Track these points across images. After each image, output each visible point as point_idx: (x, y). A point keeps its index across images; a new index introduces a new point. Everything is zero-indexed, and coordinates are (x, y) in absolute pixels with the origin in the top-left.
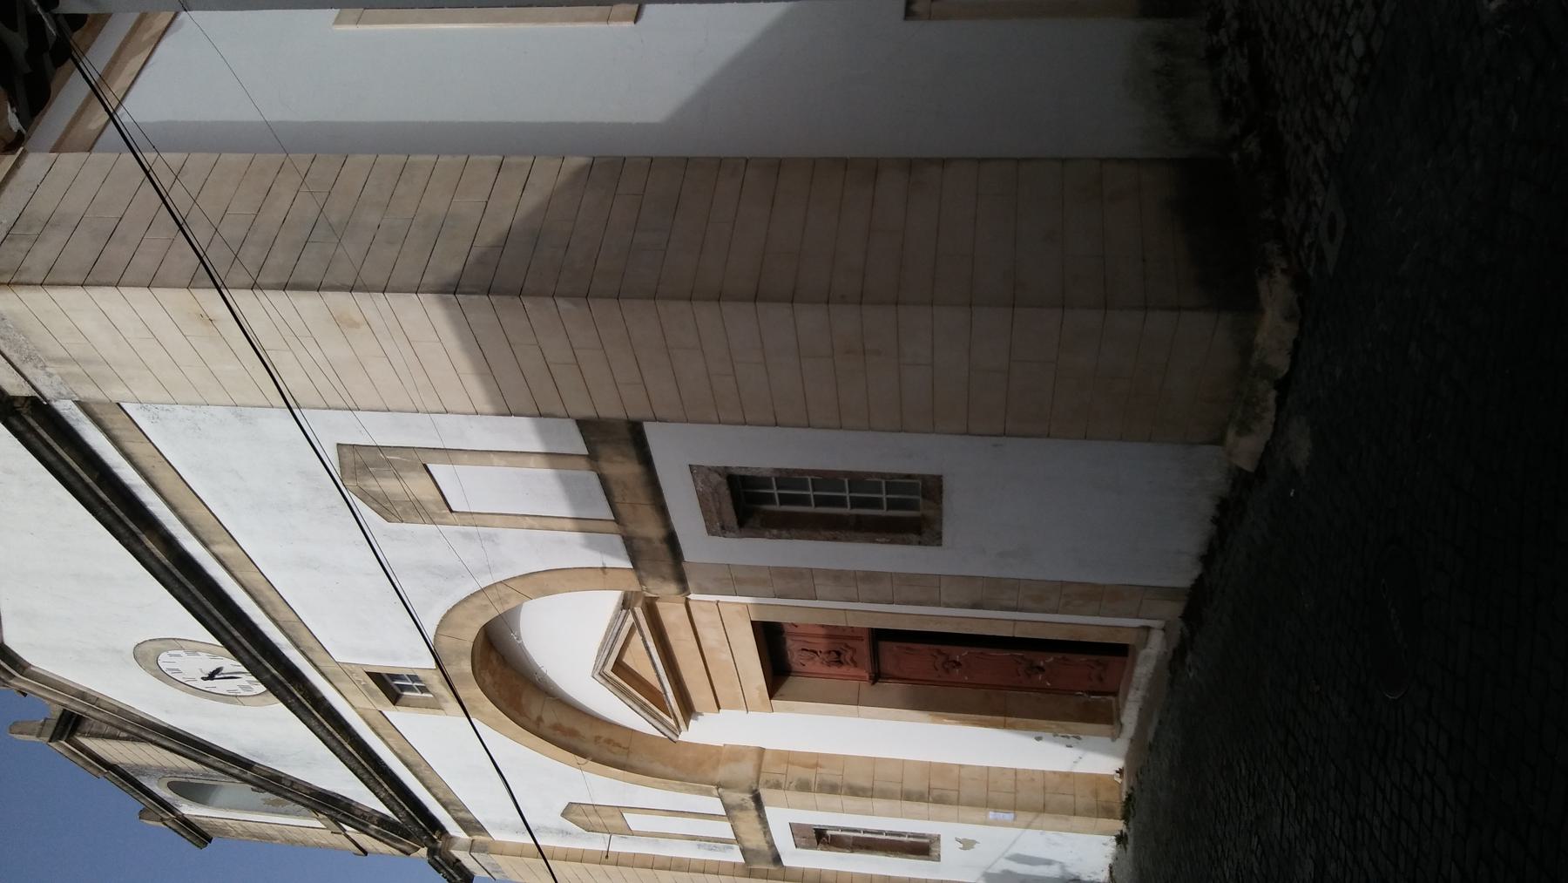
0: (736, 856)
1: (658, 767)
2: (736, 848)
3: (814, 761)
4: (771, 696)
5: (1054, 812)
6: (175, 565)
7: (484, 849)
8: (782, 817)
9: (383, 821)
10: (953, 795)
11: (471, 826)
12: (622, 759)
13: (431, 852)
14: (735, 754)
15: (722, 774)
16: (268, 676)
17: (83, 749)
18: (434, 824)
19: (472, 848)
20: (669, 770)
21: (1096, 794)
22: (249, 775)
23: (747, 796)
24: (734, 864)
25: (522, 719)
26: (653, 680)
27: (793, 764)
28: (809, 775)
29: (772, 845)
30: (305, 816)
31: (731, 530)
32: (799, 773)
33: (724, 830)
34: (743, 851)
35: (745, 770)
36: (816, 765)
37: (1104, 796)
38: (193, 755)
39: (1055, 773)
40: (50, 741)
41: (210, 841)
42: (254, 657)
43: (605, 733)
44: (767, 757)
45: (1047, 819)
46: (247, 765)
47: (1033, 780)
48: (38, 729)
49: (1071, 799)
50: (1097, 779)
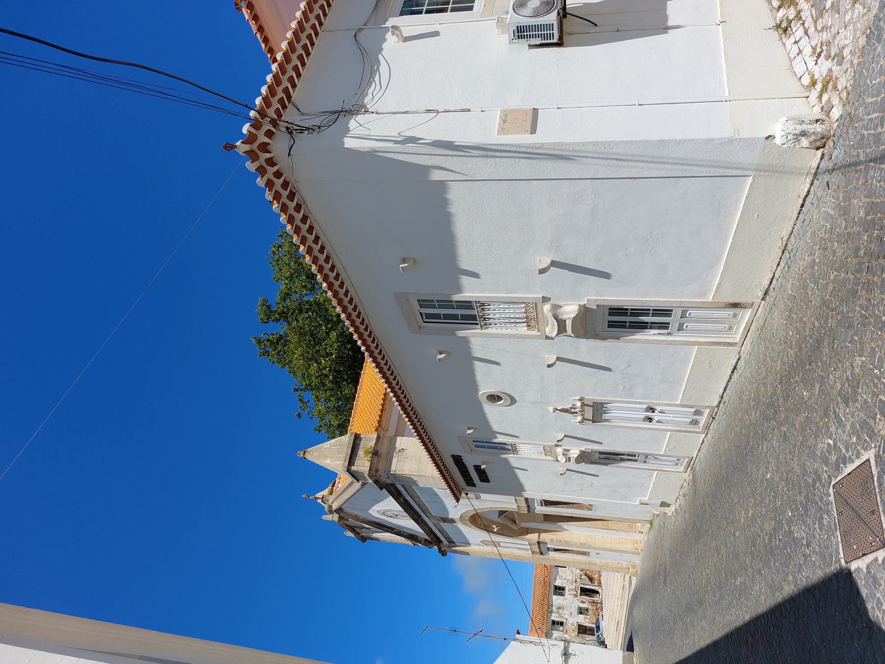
13: (440, 549)
18: (440, 541)
25: (477, 525)
33: (529, 547)
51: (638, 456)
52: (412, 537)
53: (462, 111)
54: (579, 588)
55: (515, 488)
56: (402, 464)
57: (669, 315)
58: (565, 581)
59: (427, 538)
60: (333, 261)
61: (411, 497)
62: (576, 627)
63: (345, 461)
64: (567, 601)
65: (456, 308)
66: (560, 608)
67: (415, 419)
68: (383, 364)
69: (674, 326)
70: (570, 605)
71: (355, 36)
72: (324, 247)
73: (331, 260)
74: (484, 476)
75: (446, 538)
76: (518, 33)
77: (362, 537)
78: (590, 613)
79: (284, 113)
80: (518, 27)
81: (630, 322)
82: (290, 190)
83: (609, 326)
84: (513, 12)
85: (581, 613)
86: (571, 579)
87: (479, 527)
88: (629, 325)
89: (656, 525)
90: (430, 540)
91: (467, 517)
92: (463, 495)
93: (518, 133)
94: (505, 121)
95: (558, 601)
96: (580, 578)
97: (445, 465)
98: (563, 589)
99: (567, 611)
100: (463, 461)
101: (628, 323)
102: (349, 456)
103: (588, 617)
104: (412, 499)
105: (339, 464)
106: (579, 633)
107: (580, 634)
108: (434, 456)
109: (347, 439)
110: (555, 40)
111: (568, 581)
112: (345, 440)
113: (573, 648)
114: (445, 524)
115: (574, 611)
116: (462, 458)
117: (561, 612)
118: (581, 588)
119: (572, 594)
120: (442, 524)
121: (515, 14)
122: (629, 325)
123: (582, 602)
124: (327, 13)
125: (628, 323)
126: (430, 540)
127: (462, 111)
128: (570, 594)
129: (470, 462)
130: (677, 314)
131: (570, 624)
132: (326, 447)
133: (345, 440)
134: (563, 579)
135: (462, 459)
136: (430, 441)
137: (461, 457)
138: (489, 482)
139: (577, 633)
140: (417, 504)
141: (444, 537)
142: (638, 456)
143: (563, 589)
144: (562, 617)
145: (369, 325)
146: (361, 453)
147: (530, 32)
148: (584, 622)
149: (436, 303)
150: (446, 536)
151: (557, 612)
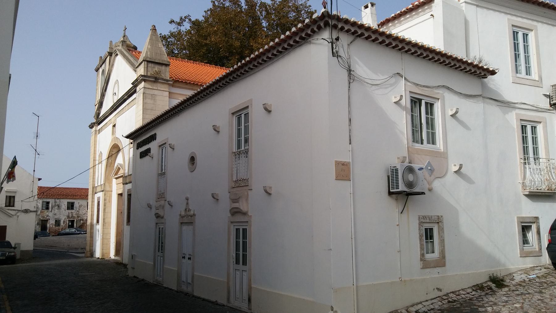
0: (96, 185)
1: (107, 172)
2: (97, 185)
3: (110, 201)
4: (118, 194)
5: (102, 246)
6: (124, 99)
7: (95, 133)
8: (100, 195)
9: (99, 114)
10: (105, 227)
11: (100, 131)
12: (108, 166)
13: (94, 123)
14: (111, 187)
15: (107, 184)
16: (114, 106)
17: (107, 56)
18: (99, 124)
19: (96, 131)
20: (107, 174)
21: (106, 253)
22: (104, 91)
23: (103, 189)
24: (95, 184)
25: (112, 149)
26: (119, 174)
27: (109, 197)
28: (107, 201)
29: (97, 193)
30: (100, 92)
31: (128, 193)
32: (108, 198)
33: (99, 184)
34: (96, 187)
35: (108, 188)
36: (109, 202)
37: (105, 255)
38: (105, 86)
39: (110, 246)
40: (108, 52)
41: (96, 72)
42: (116, 105)
43: (113, 162)
44: (111, 192)
45: (101, 245)
46: (106, 90)
47: (108, 242)
48: (111, 47)
49: (105, 249)
50: (109, 253)
51: (161, 252)
52: (101, 104)
53: (350, 140)
54: (74, 219)
55: (508, 19)
56: (150, 98)
57: (243, 264)
58: (78, 210)
59: (101, 115)
60: (290, 49)
61: (128, 104)
62: (46, 218)
63: (150, 58)
64: (64, 212)
65: (245, 136)
66: (59, 206)
67: (177, 109)
68: (233, 76)
69: (237, 267)
70: (61, 213)
71: (398, 73)
72: (286, 50)
73: (279, 54)
74: (144, 155)
75: (101, 128)
76: (395, 169)
77: (99, 69)
78: (57, 227)
79: (349, 34)
80: (398, 169)
81: (239, 241)
82: (306, 38)
83: (426, 229)
84: (407, 166)
85: (56, 221)
86: (80, 213)
87: (111, 150)
88: (244, 241)
89: (98, 260)
90: (100, 117)
91: (117, 142)
92: (132, 141)
93: (336, 173)
94: (343, 164)
95: (63, 205)
96: (80, 220)
97: (150, 129)
98: (72, 209)
99: (57, 211)
100: (153, 141)
101: (239, 240)
102: (153, 61)
103: (54, 226)
104: (127, 105)
105: (148, 54)
106: (42, 220)
107: (41, 221)
108: (164, 116)
109: (165, 59)
110: (391, 190)
111: (78, 211)
112: (165, 58)
113: (33, 215)
114: (112, 127)
115: (58, 216)
116: (155, 140)
117: (56, 208)
118: (74, 220)
119: (69, 214)
120: (111, 125)
121: (405, 167)
122: (244, 241)
123: (64, 222)
124: (414, 55)
125: (239, 240)
126: (100, 117)
127: (350, 140)
128: (69, 213)
129: (153, 146)
130: (244, 268)
131: (47, 214)
132: (159, 44)
133: (165, 58)
134: (80, 208)
135: (154, 140)
136: (170, 116)
137: (156, 140)
138: (140, 158)
139: (42, 219)
140: (124, 108)
141: (102, 127)
142: (161, 252)
143: (72, 209)
144: (52, 208)
145: (233, 82)
146: (157, 68)
147: (395, 174)
148: (50, 223)
149: (247, 124)
150: (103, 127)
151: (55, 205)
